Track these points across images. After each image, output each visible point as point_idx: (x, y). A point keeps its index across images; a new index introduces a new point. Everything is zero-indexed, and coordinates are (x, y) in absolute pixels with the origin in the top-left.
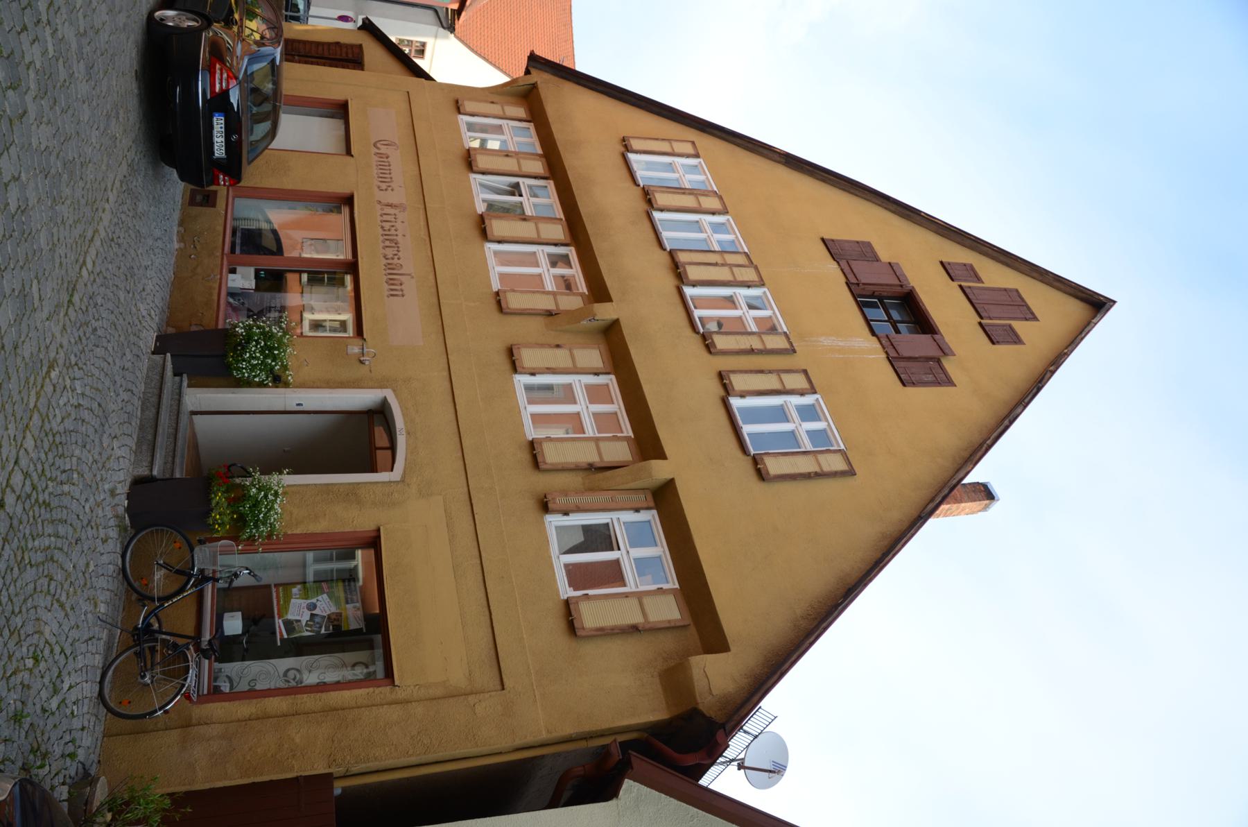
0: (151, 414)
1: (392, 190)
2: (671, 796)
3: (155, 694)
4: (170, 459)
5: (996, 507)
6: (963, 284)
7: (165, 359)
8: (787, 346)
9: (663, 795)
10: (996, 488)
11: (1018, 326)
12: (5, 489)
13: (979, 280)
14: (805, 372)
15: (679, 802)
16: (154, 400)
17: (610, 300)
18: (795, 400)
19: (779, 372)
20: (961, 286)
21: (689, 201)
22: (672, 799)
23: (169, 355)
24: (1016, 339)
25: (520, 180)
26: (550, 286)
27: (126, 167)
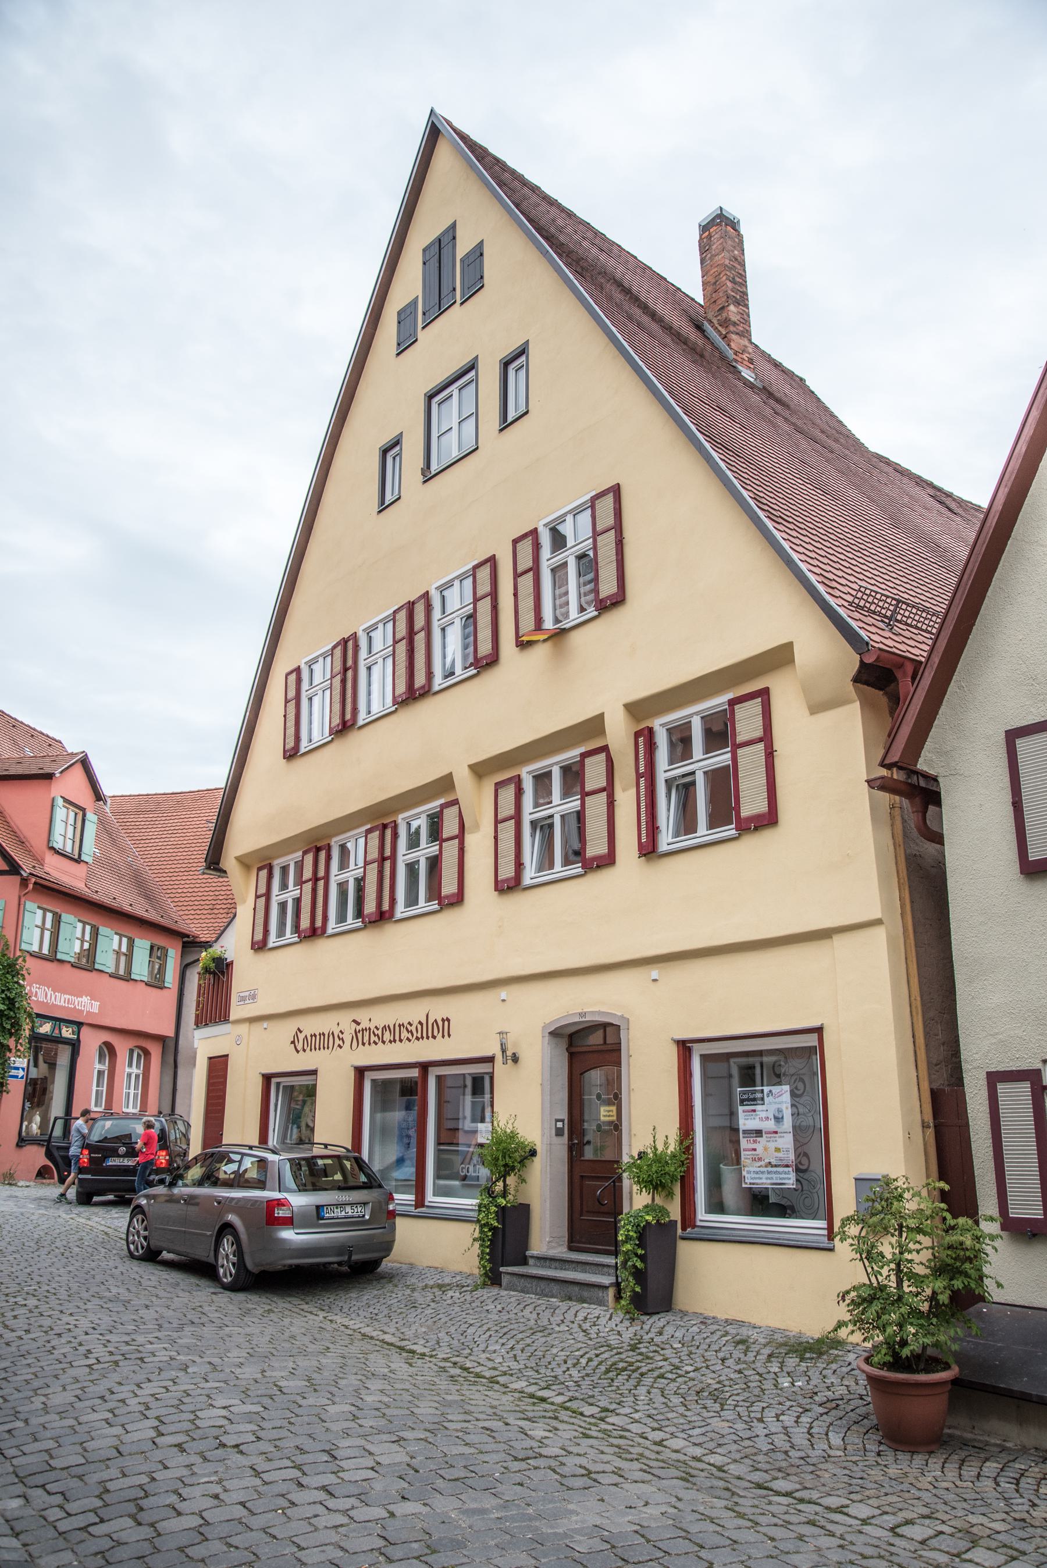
0: (555, 1288)
1: (342, 1033)
2: (937, 713)
3: (579, 1243)
4: (605, 1269)
5: (732, 210)
6: (420, 325)
7: (505, 1273)
8: (488, 566)
9: (936, 722)
10: (705, 212)
11: (463, 247)
12: (450, 1362)
13: (415, 302)
14: (515, 542)
15: (944, 703)
16: (543, 1284)
17: (601, 716)
18: (546, 552)
19: (517, 575)
20: (423, 328)
21: (420, 639)
22: (940, 712)
23: (502, 1269)
24: (478, 253)
25: (661, 778)
26: (722, 758)
27: (520, 1382)
